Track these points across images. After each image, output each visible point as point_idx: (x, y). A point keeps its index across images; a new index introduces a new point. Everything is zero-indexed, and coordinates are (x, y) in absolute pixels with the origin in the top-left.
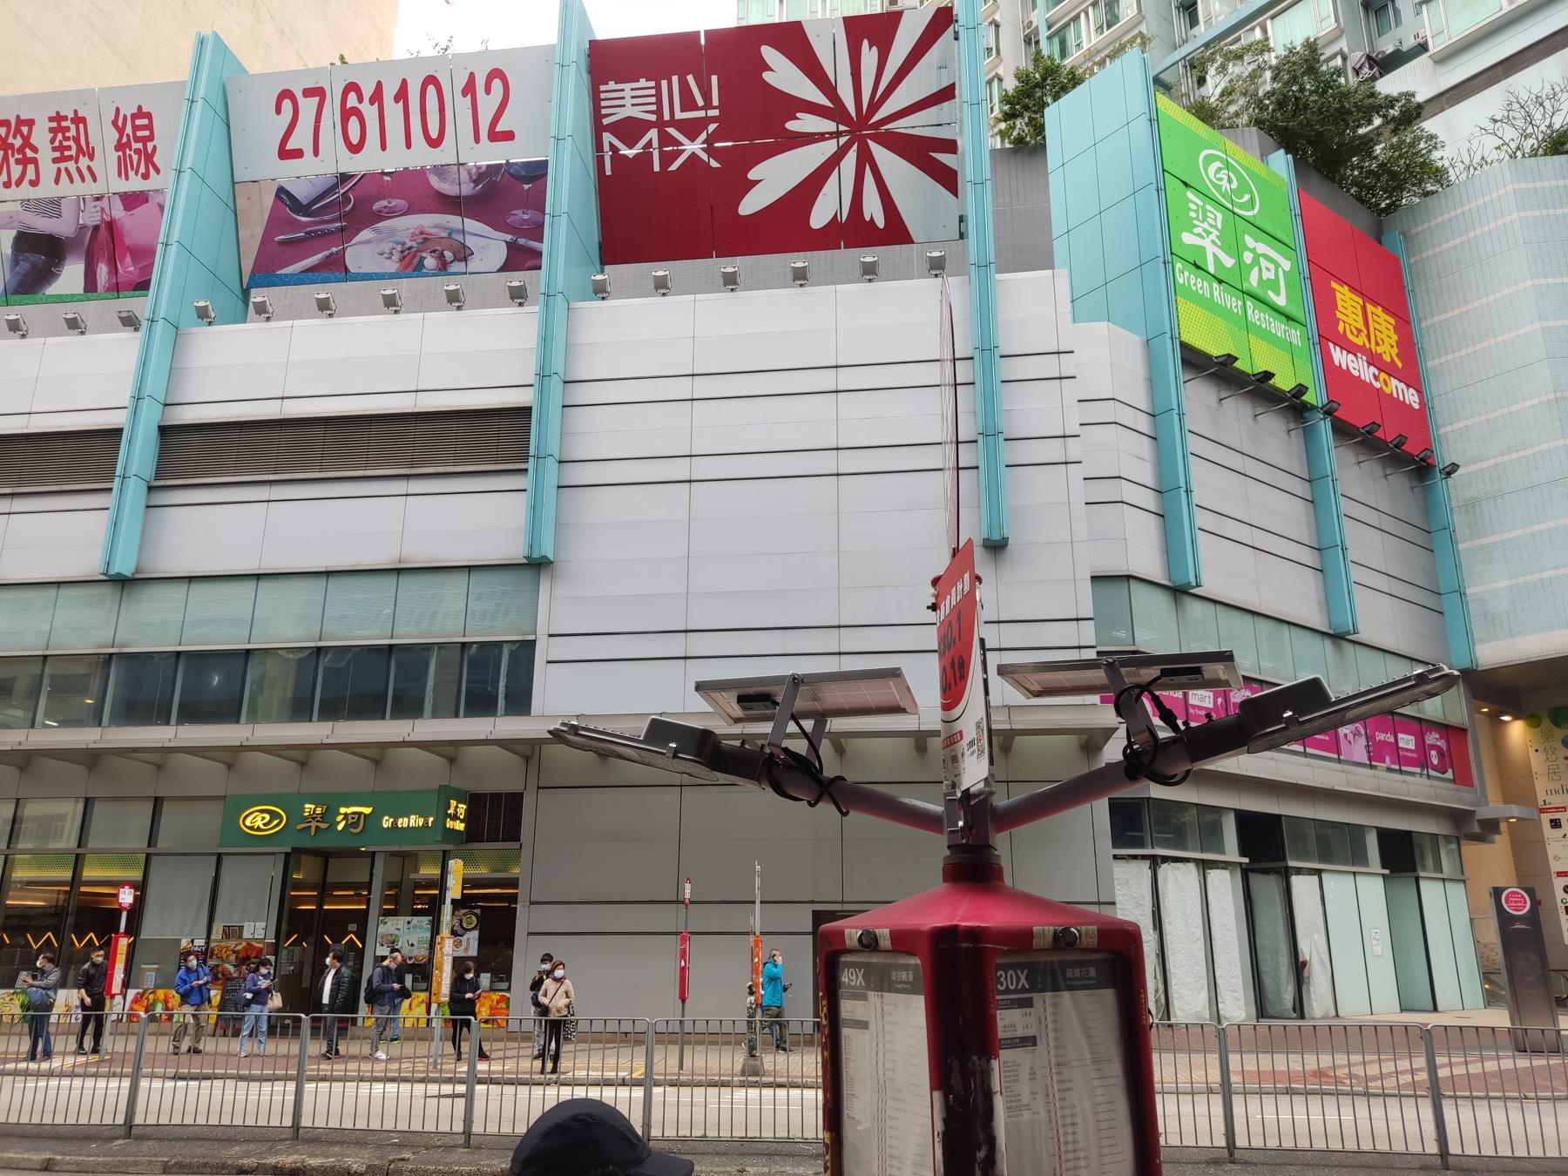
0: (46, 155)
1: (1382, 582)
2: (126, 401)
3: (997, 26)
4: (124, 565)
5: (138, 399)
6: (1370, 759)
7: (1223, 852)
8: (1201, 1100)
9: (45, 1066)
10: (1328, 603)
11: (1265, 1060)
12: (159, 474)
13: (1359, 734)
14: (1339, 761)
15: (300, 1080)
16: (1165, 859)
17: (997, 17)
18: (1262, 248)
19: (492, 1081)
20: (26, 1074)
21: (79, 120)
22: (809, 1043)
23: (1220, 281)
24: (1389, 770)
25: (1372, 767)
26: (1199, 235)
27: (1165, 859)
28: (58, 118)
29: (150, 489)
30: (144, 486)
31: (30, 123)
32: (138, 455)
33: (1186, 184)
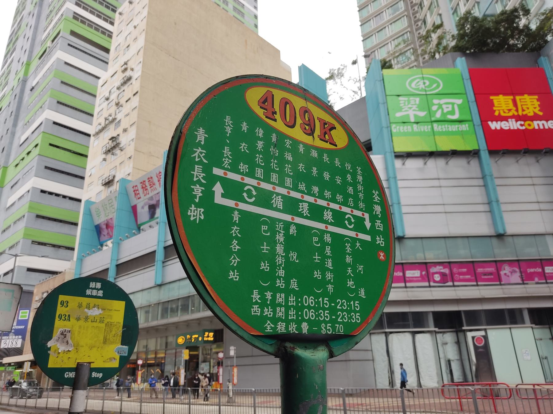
0: (148, 187)
1: (535, 206)
2: (156, 243)
3: (440, 15)
4: (159, 282)
5: (158, 242)
6: (523, 280)
7: (428, 327)
8: (250, 408)
9: (207, 402)
10: (494, 223)
11: (422, 401)
12: (165, 258)
13: (515, 272)
14: (501, 285)
15: (164, 403)
16: (391, 333)
17: (440, 12)
18: (443, 101)
19: (195, 404)
20: (203, 405)
21: (151, 178)
22: (278, 395)
23: (417, 123)
24: (537, 283)
25: (524, 284)
26: (406, 111)
27: (391, 333)
28: (148, 179)
29: (163, 262)
30: (161, 263)
31: (144, 181)
32: (160, 256)
33: (398, 96)
